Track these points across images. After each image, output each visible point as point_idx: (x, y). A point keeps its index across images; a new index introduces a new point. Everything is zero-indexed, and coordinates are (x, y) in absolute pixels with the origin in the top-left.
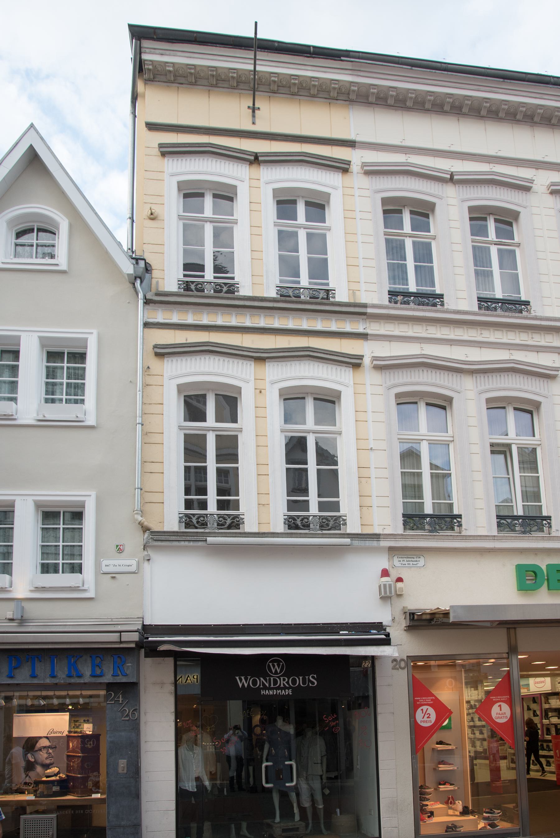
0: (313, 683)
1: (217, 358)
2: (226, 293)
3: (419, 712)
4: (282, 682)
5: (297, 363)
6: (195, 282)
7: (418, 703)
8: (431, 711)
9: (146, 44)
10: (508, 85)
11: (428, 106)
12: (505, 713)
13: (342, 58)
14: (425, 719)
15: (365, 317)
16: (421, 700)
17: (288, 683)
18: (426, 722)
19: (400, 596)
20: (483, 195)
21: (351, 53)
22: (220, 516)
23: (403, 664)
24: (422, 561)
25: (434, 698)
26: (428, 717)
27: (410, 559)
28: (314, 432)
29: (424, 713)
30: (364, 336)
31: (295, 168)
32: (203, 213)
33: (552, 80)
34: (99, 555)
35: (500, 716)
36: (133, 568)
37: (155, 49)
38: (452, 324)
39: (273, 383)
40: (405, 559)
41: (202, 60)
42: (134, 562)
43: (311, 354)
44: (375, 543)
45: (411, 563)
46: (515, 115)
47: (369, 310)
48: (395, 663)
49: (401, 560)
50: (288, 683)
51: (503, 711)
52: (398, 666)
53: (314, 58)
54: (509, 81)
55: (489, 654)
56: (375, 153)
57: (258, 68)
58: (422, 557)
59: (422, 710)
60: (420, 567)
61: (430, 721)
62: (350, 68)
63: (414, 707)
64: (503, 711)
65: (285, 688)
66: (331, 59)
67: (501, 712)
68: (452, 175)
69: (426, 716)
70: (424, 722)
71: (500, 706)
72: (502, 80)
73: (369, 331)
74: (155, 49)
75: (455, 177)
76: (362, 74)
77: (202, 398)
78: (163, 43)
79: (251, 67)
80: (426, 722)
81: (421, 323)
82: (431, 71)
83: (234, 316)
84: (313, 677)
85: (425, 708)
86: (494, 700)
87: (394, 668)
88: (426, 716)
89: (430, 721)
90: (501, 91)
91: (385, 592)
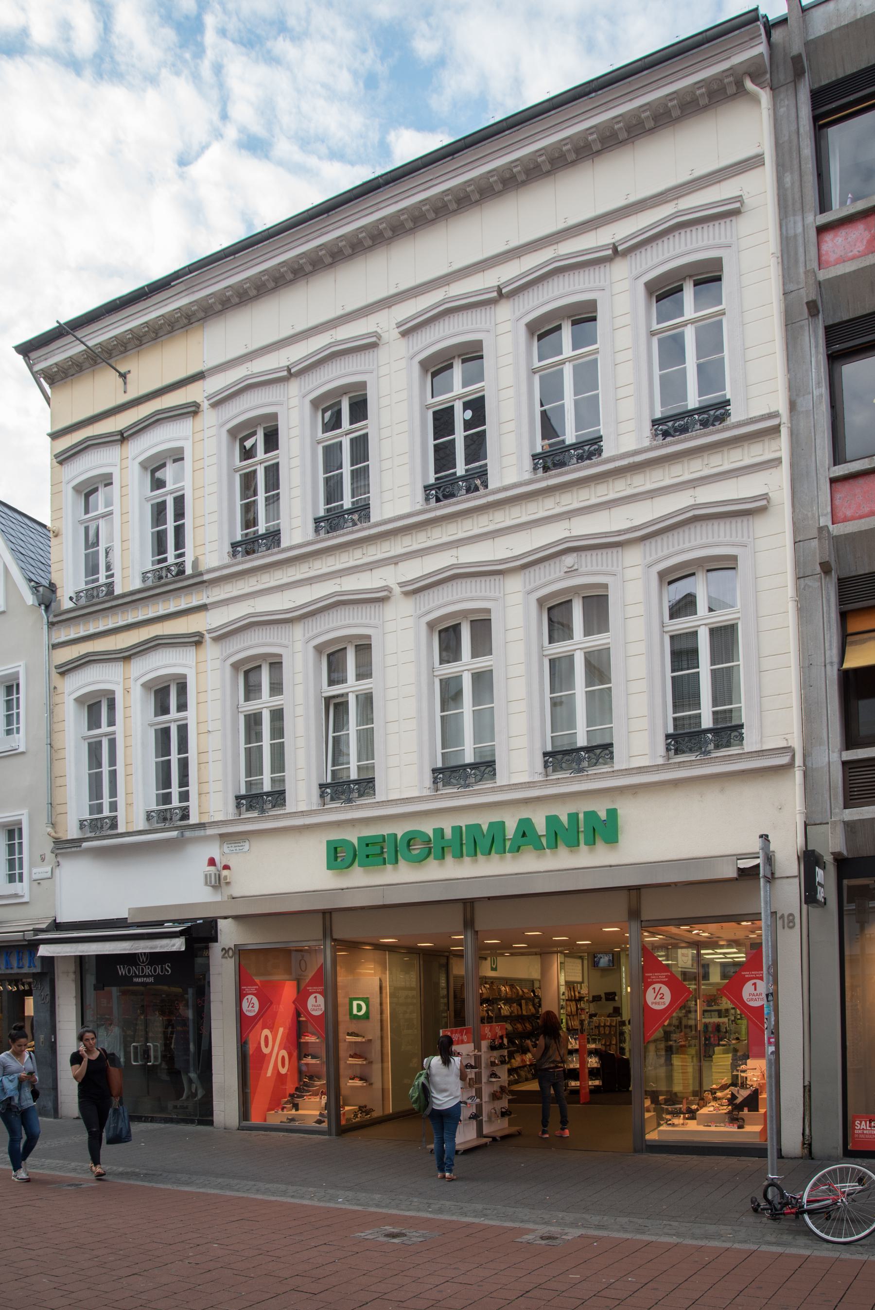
0: (168, 972)
1: (98, 665)
2: (106, 595)
3: (245, 1001)
4: (147, 971)
5: (153, 653)
6: (441, 487)
7: (649, 980)
8: (665, 990)
9: (33, 355)
10: (335, 216)
11: (597, 147)
12: (320, 1005)
13: (173, 284)
14: (658, 1000)
15: (206, 584)
16: (652, 976)
17: (151, 971)
18: (249, 1011)
19: (228, 883)
20: (429, 341)
21: (180, 273)
22: (92, 820)
23: (231, 953)
24: (246, 846)
25: (669, 974)
26: (661, 998)
27: (237, 845)
28: (175, 721)
29: (656, 992)
30: (203, 608)
31: (155, 429)
32: (452, 391)
33: (381, 180)
34: (32, 865)
35: (754, 997)
36: (49, 875)
37: (40, 357)
38: (685, 457)
39: (136, 680)
40: (233, 845)
41: (351, 225)
42: (49, 869)
43: (160, 642)
44: (201, 833)
45: (238, 848)
46: (723, 89)
47: (206, 577)
48: (224, 951)
49: (230, 846)
50: (151, 971)
51: (318, 1003)
52: (226, 955)
53: (150, 297)
54: (333, 212)
55: (301, 941)
56: (412, 301)
57: (90, 344)
58: (247, 843)
59: (654, 989)
60: (245, 852)
61: (664, 1003)
62: (184, 288)
63: (240, 996)
64: (318, 1003)
65: (149, 976)
66: (164, 290)
67: (755, 993)
68: (499, 290)
69: (659, 996)
70: (656, 1003)
71: (315, 997)
72: (325, 216)
73: (207, 601)
74: (40, 357)
75: (620, 248)
76: (195, 289)
77: (455, 630)
78: (43, 349)
79: (84, 348)
80: (658, 1003)
81: (319, 557)
82: (253, 248)
83: (120, 615)
84: (168, 966)
85: (657, 986)
86: (746, 976)
87: (223, 957)
88: (659, 996)
89: (664, 1003)
90: (331, 227)
91: (216, 883)
